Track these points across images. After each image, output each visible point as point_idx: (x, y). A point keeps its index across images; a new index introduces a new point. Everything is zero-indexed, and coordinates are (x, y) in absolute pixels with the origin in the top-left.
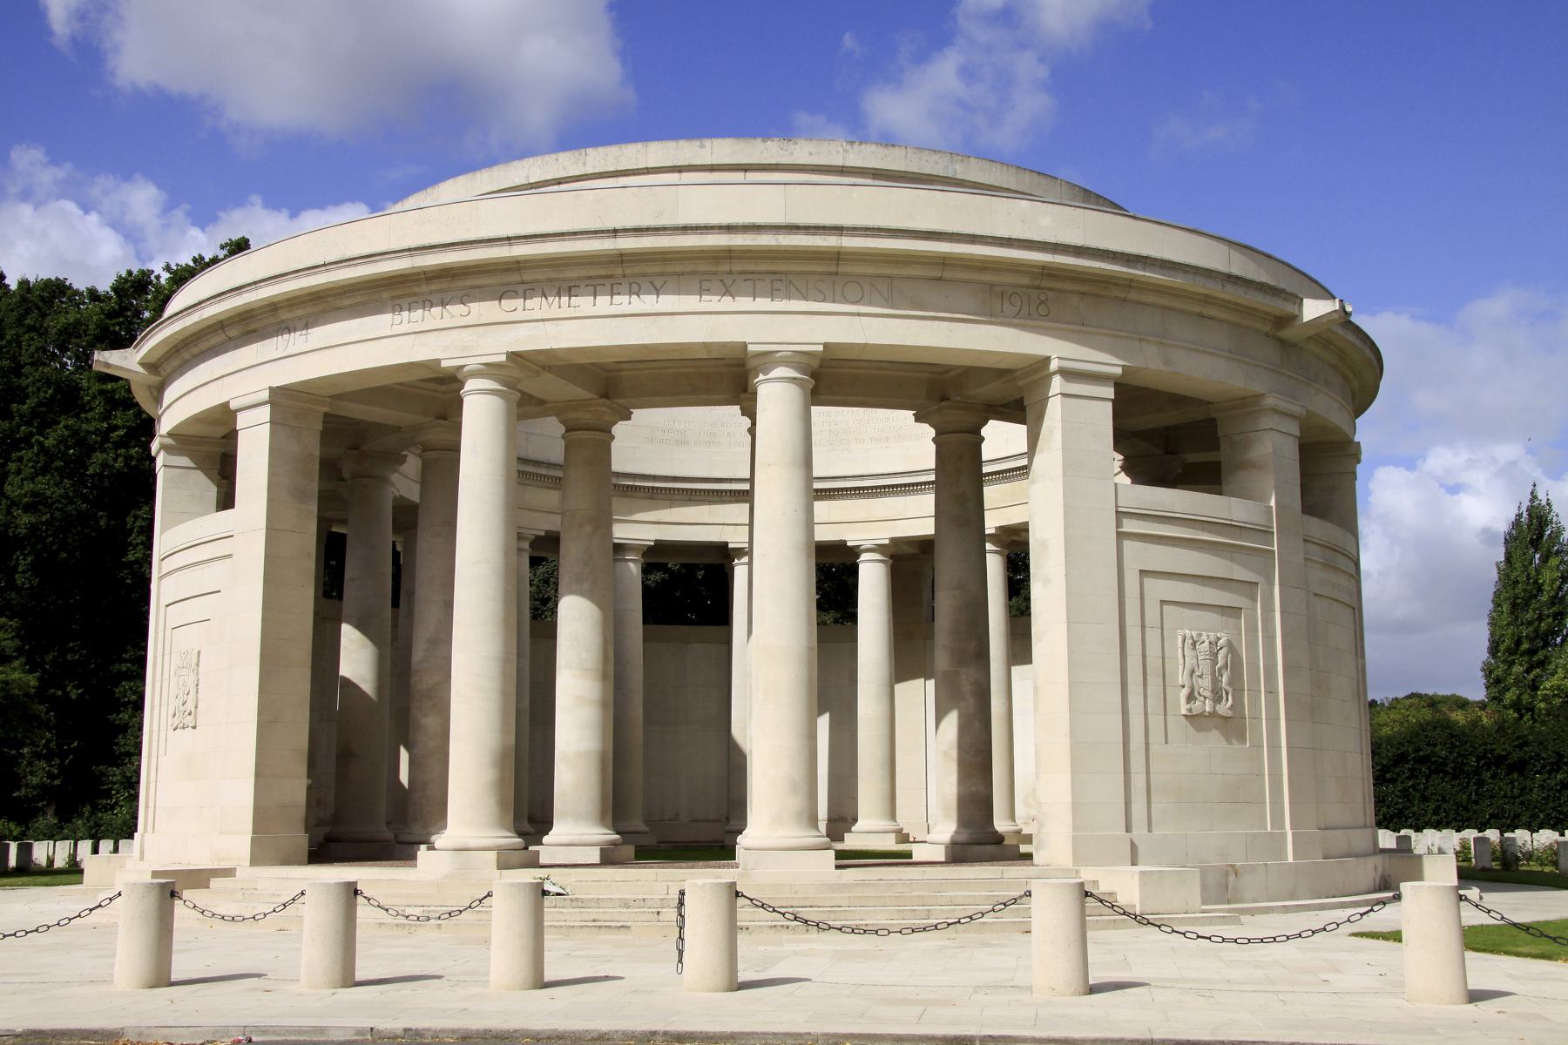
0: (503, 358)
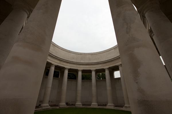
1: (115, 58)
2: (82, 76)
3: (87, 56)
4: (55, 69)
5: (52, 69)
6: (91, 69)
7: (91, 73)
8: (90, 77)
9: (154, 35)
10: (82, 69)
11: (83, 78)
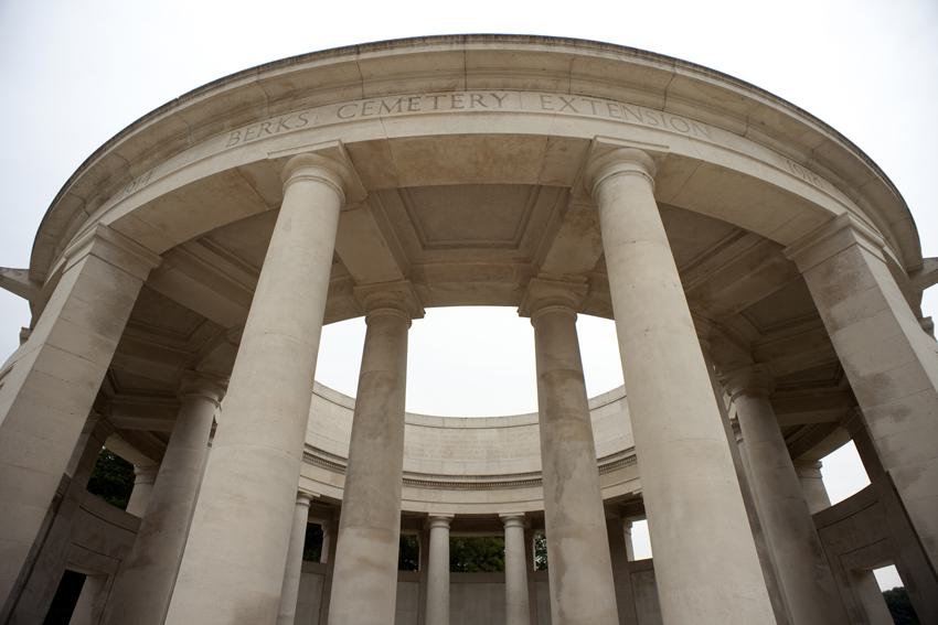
0: (337, 144)
1: (623, 452)
2: (452, 542)
3: (480, 435)
4: (311, 514)
5: (440, 539)
6: (502, 511)
7: (504, 531)
8: (494, 549)
9: (741, 440)
10: (452, 511)
11: (459, 560)
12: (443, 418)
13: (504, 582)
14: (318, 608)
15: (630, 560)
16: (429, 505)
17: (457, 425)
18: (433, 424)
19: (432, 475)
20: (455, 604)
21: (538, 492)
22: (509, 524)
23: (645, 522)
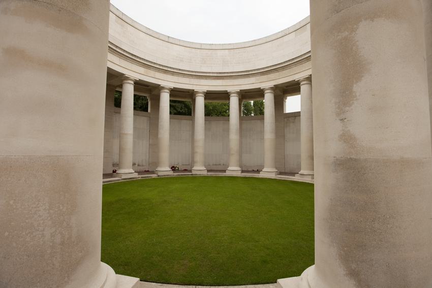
6: (229, 89)
10: (206, 89)
11: (209, 112)
12: (201, 44)
13: (229, 121)
14: (148, 130)
15: (284, 112)
16: (195, 86)
17: (208, 47)
18: (197, 47)
19: (195, 72)
20: (207, 129)
21: (308, 65)
22: (266, 92)
23: (299, 96)
